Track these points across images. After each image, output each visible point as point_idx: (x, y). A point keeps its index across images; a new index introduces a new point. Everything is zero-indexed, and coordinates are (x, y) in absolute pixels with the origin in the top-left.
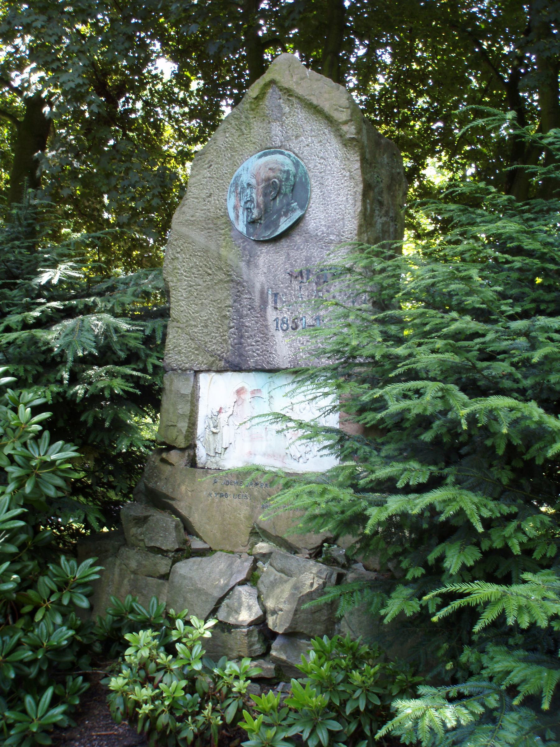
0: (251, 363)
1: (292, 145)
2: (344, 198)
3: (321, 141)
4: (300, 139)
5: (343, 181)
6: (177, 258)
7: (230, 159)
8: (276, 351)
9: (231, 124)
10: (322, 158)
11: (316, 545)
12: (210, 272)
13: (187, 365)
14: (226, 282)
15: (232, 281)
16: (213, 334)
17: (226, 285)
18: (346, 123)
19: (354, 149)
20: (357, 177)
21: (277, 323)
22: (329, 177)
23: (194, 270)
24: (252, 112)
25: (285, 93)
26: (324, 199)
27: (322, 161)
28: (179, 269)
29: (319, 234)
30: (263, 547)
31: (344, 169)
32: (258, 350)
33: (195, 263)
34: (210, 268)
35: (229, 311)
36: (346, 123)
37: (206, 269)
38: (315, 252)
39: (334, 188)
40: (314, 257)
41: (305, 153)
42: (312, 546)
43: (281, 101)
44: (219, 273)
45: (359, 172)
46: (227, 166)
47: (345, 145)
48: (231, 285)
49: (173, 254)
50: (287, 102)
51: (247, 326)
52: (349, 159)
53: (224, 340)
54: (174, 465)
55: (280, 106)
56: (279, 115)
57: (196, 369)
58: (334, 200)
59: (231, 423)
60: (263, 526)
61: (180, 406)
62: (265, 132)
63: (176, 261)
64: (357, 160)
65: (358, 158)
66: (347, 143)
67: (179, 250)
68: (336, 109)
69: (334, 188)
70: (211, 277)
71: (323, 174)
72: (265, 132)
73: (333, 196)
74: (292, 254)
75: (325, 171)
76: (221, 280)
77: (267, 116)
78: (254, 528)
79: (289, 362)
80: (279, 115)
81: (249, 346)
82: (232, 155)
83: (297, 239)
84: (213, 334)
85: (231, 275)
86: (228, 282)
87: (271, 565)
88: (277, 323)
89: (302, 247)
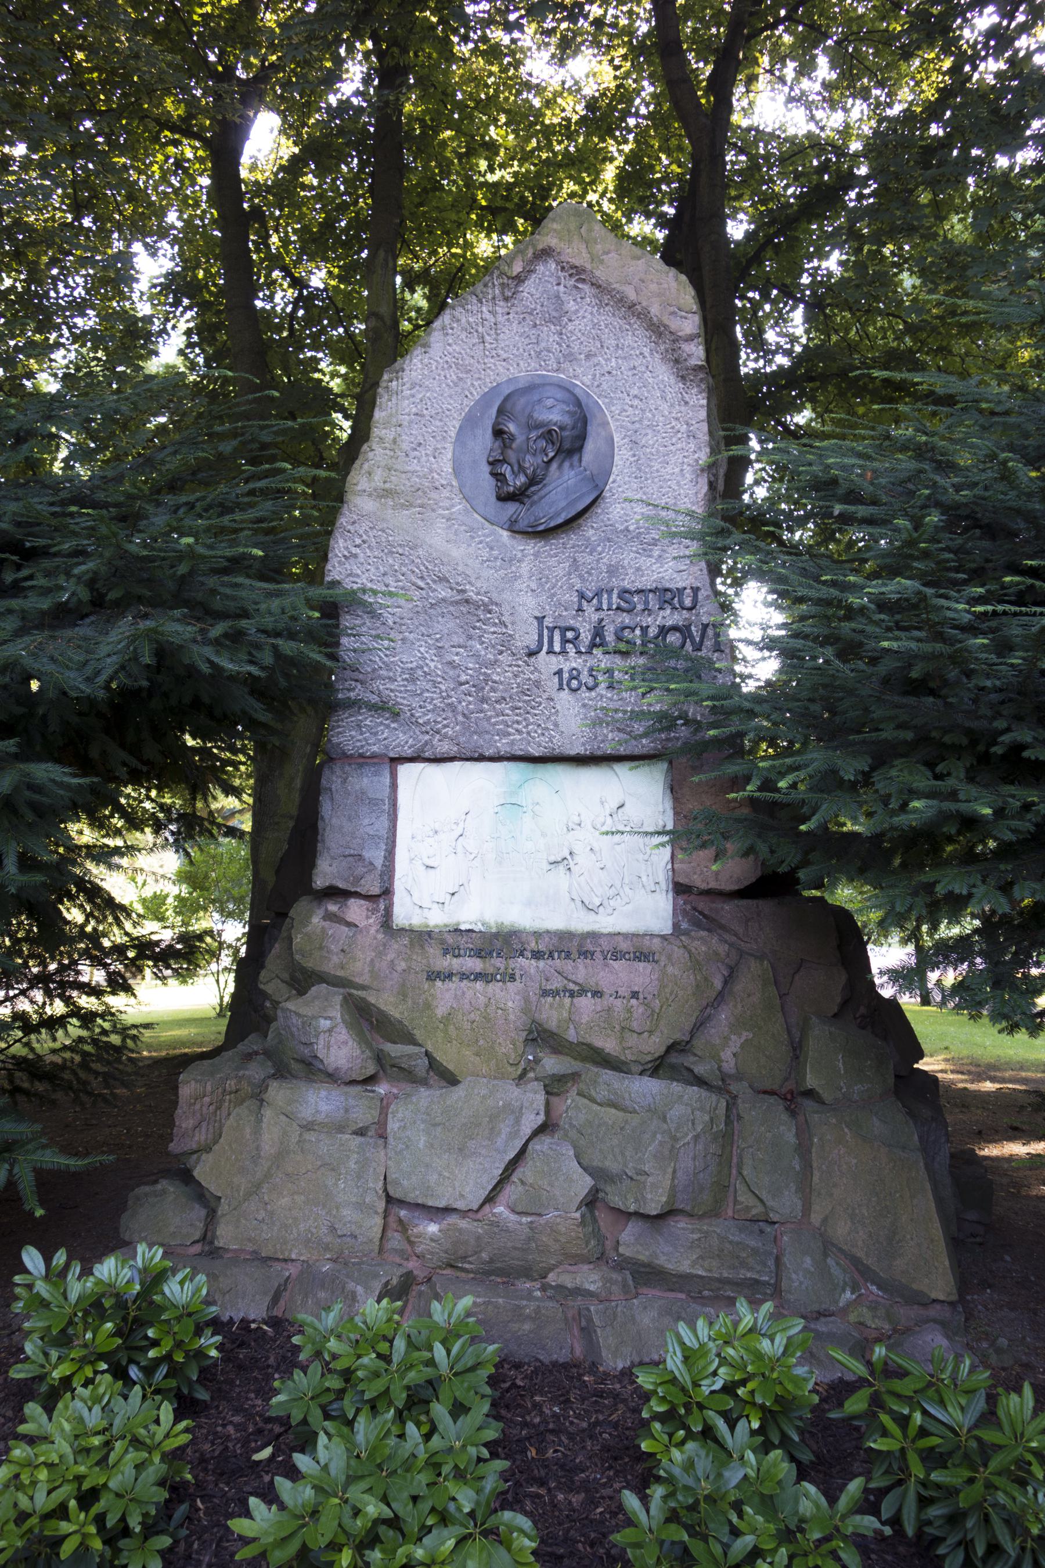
0: (502, 745)
1: (579, 371)
2: (677, 470)
3: (634, 368)
4: (595, 360)
5: (674, 440)
6: (355, 556)
7: (456, 385)
8: (556, 725)
9: (458, 321)
10: (636, 396)
11: (657, 1055)
12: (421, 584)
13: (375, 748)
14: (452, 603)
15: (467, 601)
16: (426, 695)
17: (452, 608)
18: (690, 338)
19: (698, 386)
20: (700, 435)
21: (561, 679)
22: (649, 431)
23: (390, 580)
24: (502, 303)
25: (571, 275)
26: (640, 469)
27: (636, 402)
28: (358, 576)
29: (632, 528)
30: (552, 1064)
31: (677, 419)
32: (518, 722)
33: (392, 566)
34: (422, 578)
35: (457, 654)
36: (690, 338)
37: (414, 579)
38: (628, 557)
39: (658, 451)
40: (623, 567)
41: (605, 386)
42: (649, 1058)
43: (561, 288)
44: (438, 587)
45: (705, 427)
46: (451, 396)
47: (683, 378)
48: (464, 609)
49: (347, 548)
50: (574, 292)
51: (495, 682)
52: (686, 403)
53: (449, 705)
54: (356, 926)
55: (558, 297)
56: (554, 314)
57: (392, 755)
58: (658, 471)
59: (460, 849)
60: (552, 1025)
61: (366, 821)
62: (527, 341)
63: (352, 560)
64: (702, 406)
65: (704, 402)
66: (684, 374)
67: (358, 541)
68: (673, 313)
69: (658, 451)
70: (423, 592)
71: (637, 425)
72: (527, 341)
73: (656, 466)
74: (581, 560)
75: (640, 421)
76: (444, 600)
77: (531, 314)
78: (530, 1032)
79: (583, 744)
80: (554, 314)
81: (498, 715)
82: (460, 379)
83: (590, 530)
84: (426, 695)
85: (463, 591)
86: (457, 603)
87: (580, 1094)
88: (561, 679)
89: (599, 549)
